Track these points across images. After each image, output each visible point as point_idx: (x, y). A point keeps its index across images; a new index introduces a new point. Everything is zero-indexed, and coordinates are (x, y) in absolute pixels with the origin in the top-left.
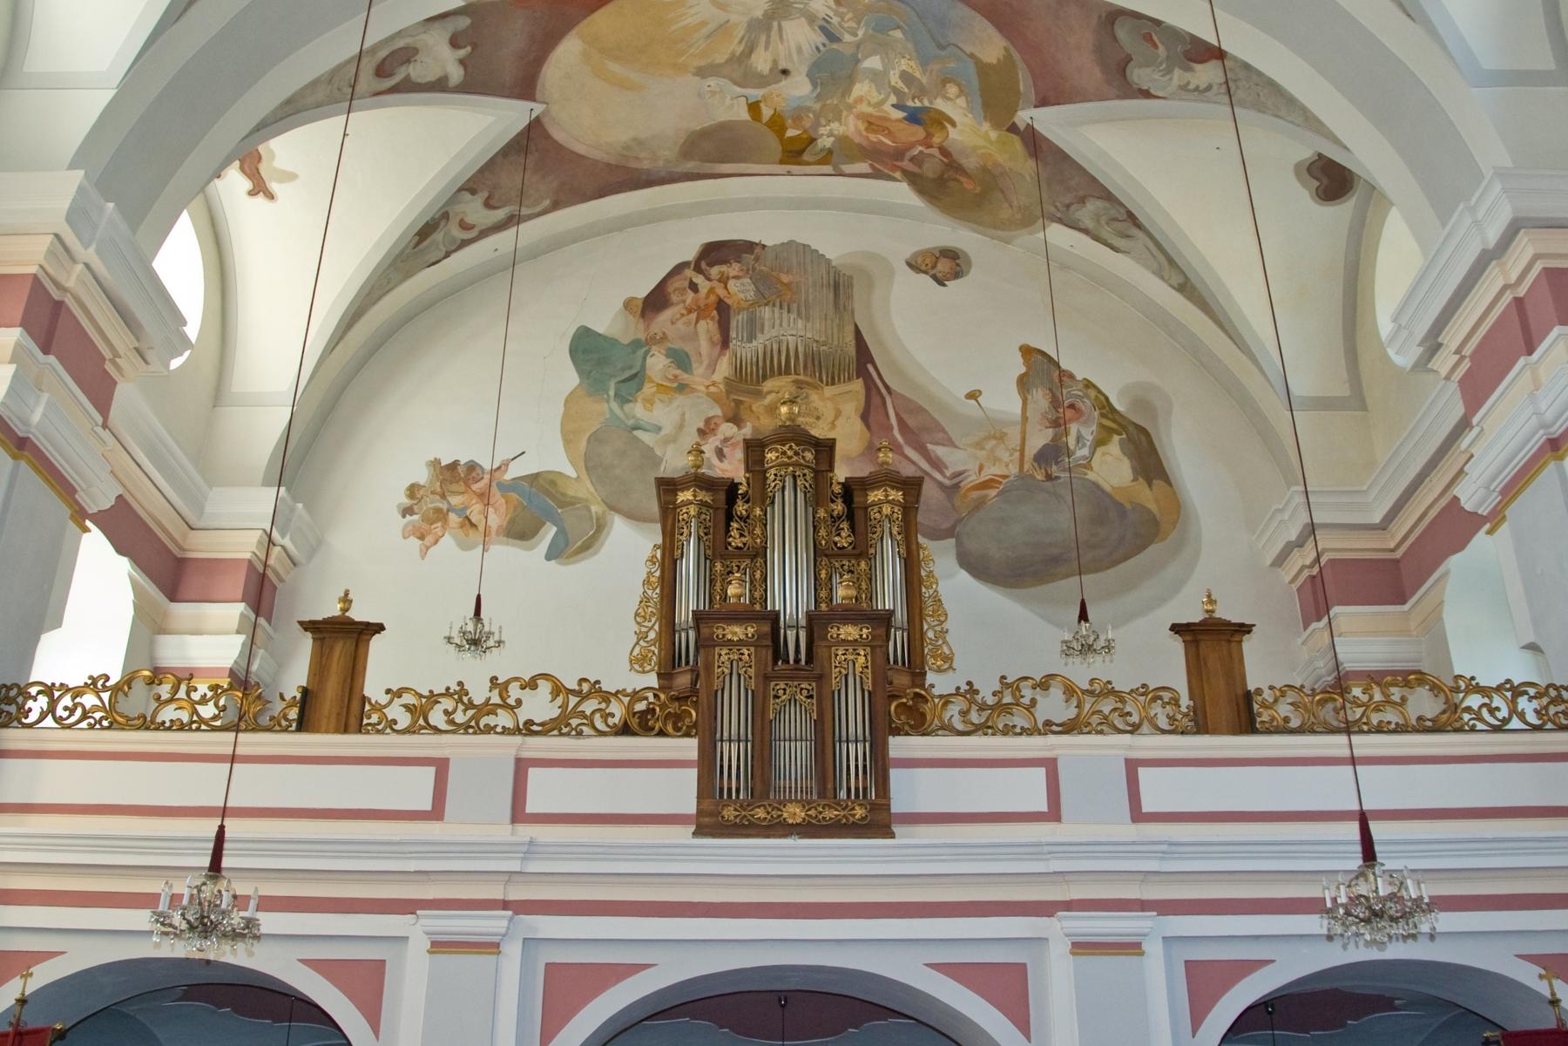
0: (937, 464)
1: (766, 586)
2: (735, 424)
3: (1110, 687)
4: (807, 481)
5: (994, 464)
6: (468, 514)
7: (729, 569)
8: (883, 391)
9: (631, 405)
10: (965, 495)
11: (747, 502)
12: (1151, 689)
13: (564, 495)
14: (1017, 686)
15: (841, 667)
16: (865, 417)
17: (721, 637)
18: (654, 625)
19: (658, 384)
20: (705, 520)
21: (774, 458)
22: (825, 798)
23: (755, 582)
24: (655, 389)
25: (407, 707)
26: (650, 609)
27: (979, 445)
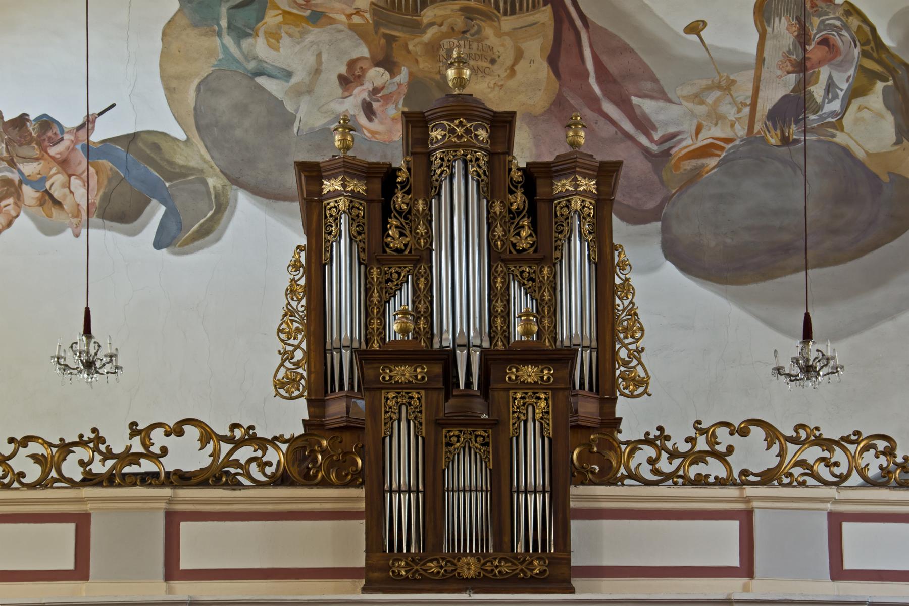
0: (644, 124)
1: (432, 297)
2: (386, 69)
3: (817, 433)
4: (480, 167)
5: (716, 124)
6: (48, 187)
7: (388, 276)
8: (578, 23)
9: (250, 40)
10: (677, 167)
11: (408, 193)
12: (864, 436)
13: (171, 163)
14: (713, 432)
15: (520, 412)
16: (553, 60)
17: (387, 378)
18: (301, 342)
19: (285, 13)
20: (358, 216)
21: (440, 137)
23: (419, 293)
25: (36, 458)
26: (296, 325)
27: (698, 98)
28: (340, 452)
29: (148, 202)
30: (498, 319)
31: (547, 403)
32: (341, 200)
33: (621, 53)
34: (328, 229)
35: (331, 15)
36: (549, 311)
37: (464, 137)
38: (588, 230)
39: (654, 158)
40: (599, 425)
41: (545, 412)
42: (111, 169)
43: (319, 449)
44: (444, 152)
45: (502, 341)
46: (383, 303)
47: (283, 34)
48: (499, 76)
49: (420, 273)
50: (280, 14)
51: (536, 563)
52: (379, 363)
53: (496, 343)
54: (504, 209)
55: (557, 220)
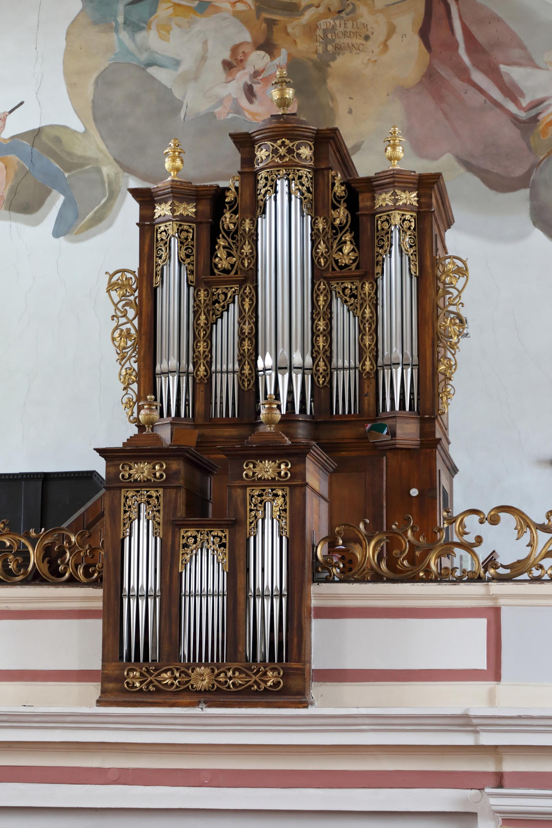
4: (303, 185)
7: (215, 298)
9: (143, 34)
11: (235, 212)
13: (70, 154)
21: (264, 158)
22: (235, 661)
23: (244, 313)
24: (171, 11)
28: (87, 548)
29: (49, 192)
30: (320, 338)
31: (284, 500)
32: (170, 224)
33: (490, 23)
34: (159, 253)
35: (216, 4)
36: (370, 329)
37: (287, 156)
38: (408, 243)
39: (522, 125)
40: (419, 446)
41: (283, 510)
42: (18, 163)
43: (67, 544)
44: (268, 172)
45: (324, 361)
46: (209, 325)
47: (174, 26)
48: (373, 52)
49: (204, 330)
50: (171, 7)
51: (270, 674)
52: (119, 460)
53: (318, 363)
54: (327, 225)
55: (378, 234)
